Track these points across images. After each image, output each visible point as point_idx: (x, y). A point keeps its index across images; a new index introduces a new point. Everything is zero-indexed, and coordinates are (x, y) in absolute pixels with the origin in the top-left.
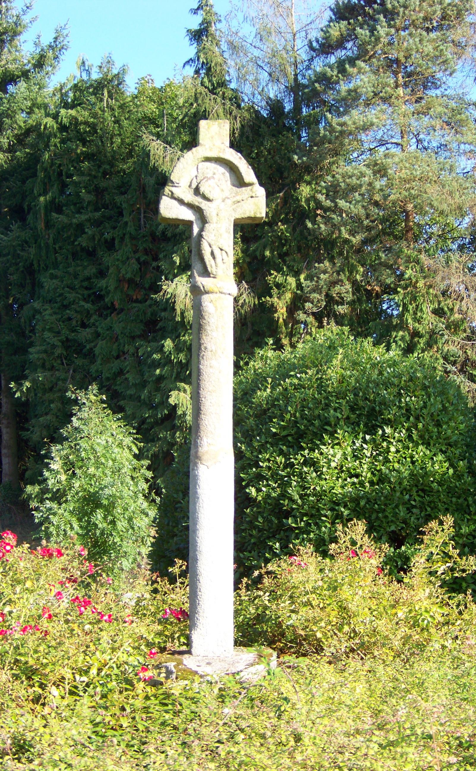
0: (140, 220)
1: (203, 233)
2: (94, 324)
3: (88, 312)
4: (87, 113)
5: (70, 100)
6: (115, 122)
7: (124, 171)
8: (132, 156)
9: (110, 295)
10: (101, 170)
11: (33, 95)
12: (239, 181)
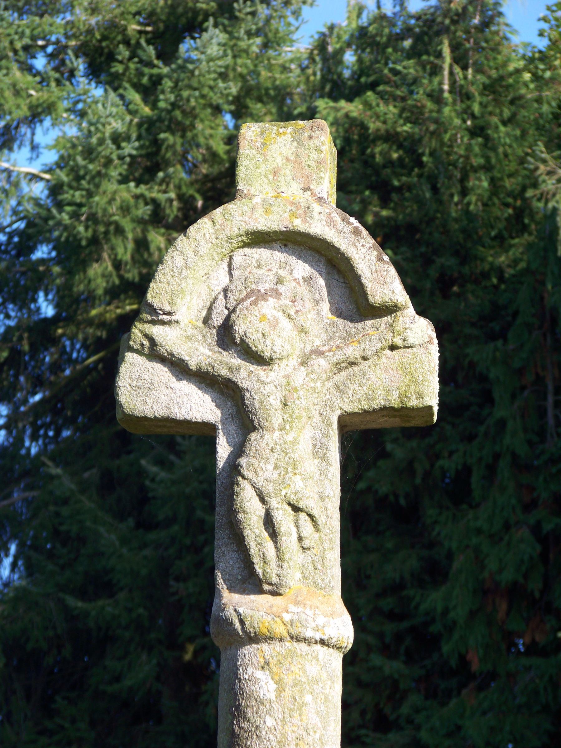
0: (542, 413)
1: (243, 461)
2: (410, 721)
3: (395, 684)
4: (393, 109)
5: (347, 73)
6: (474, 132)
7: (500, 272)
8: (525, 228)
9: (456, 636)
10: (433, 272)
11: (244, 65)
12: (354, 303)
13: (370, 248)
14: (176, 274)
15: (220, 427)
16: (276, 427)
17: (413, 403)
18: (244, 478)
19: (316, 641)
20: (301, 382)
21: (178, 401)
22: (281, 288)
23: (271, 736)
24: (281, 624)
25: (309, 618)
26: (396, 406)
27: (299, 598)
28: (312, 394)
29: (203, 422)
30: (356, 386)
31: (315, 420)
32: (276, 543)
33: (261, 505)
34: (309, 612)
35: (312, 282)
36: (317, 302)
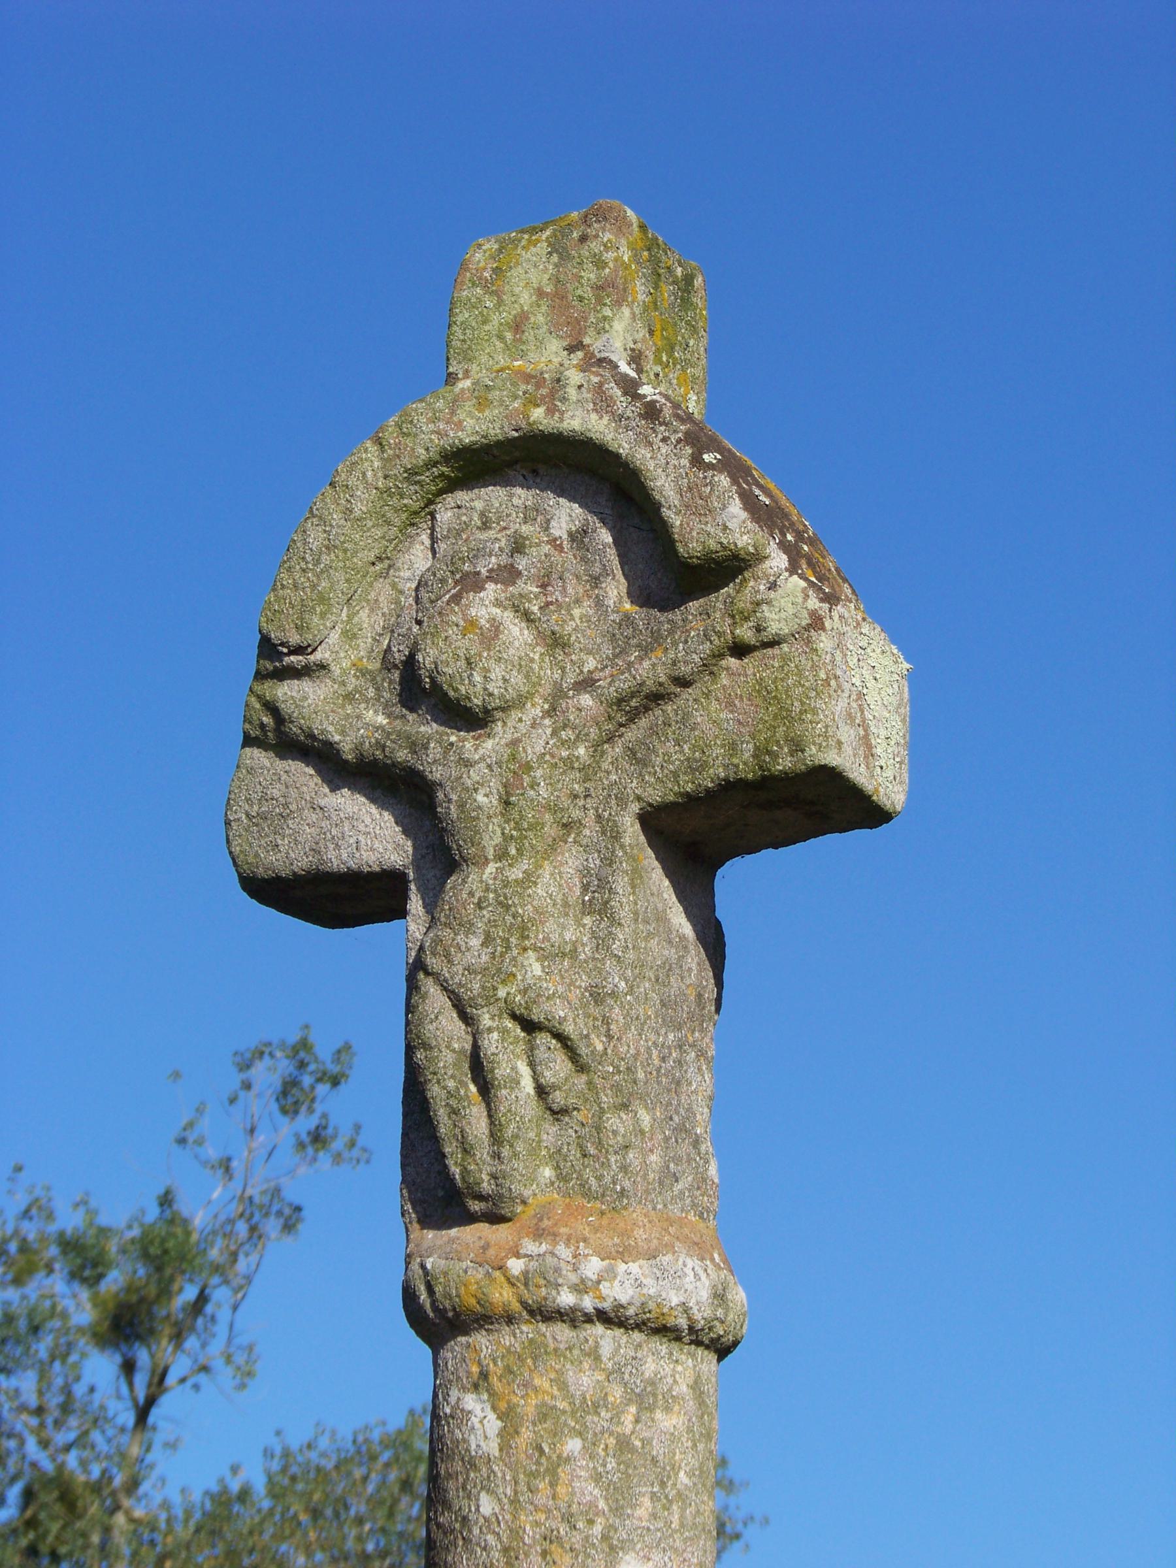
13: (679, 441)
14: (310, 566)
15: (411, 876)
16: (490, 853)
17: (785, 763)
18: (427, 974)
19: (586, 1314)
20: (539, 749)
21: (334, 832)
22: (522, 563)
23: (490, 1538)
24: (506, 1285)
25: (563, 1264)
26: (750, 776)
27: (546, 1223)
28: (564, 772)
29: (384, 871)
30: (670, 746)
31: (587, 832)
32: (488, 1105)
33: (463, 1027)
34: (564, 1252)
35: (586, 540)
36: (596, 581)
